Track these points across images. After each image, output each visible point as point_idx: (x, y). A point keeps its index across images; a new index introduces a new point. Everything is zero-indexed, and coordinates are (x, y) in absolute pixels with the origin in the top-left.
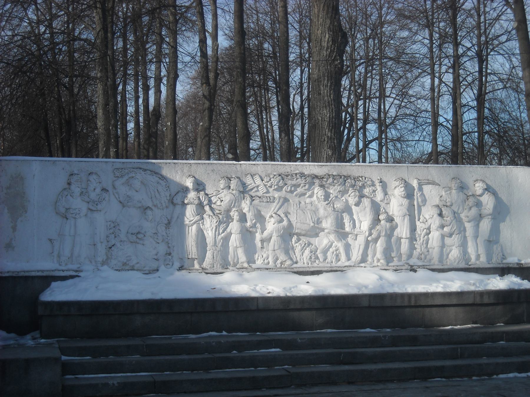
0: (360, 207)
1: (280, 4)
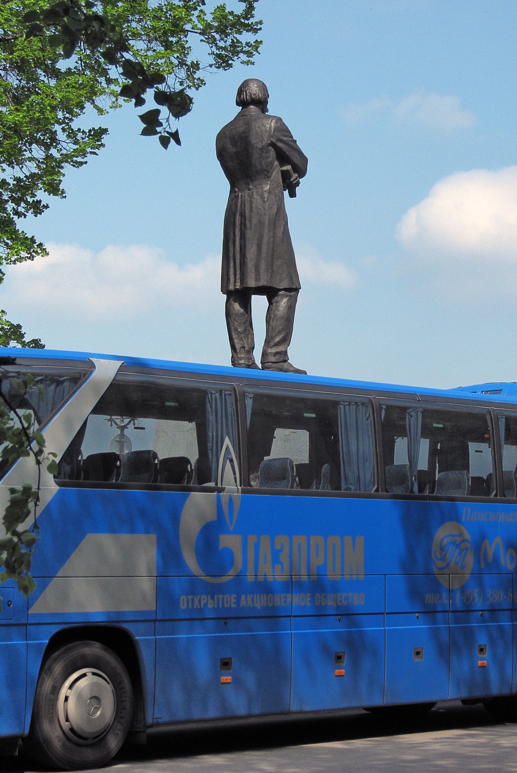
0: (30, 457)
1: (516, 764)
